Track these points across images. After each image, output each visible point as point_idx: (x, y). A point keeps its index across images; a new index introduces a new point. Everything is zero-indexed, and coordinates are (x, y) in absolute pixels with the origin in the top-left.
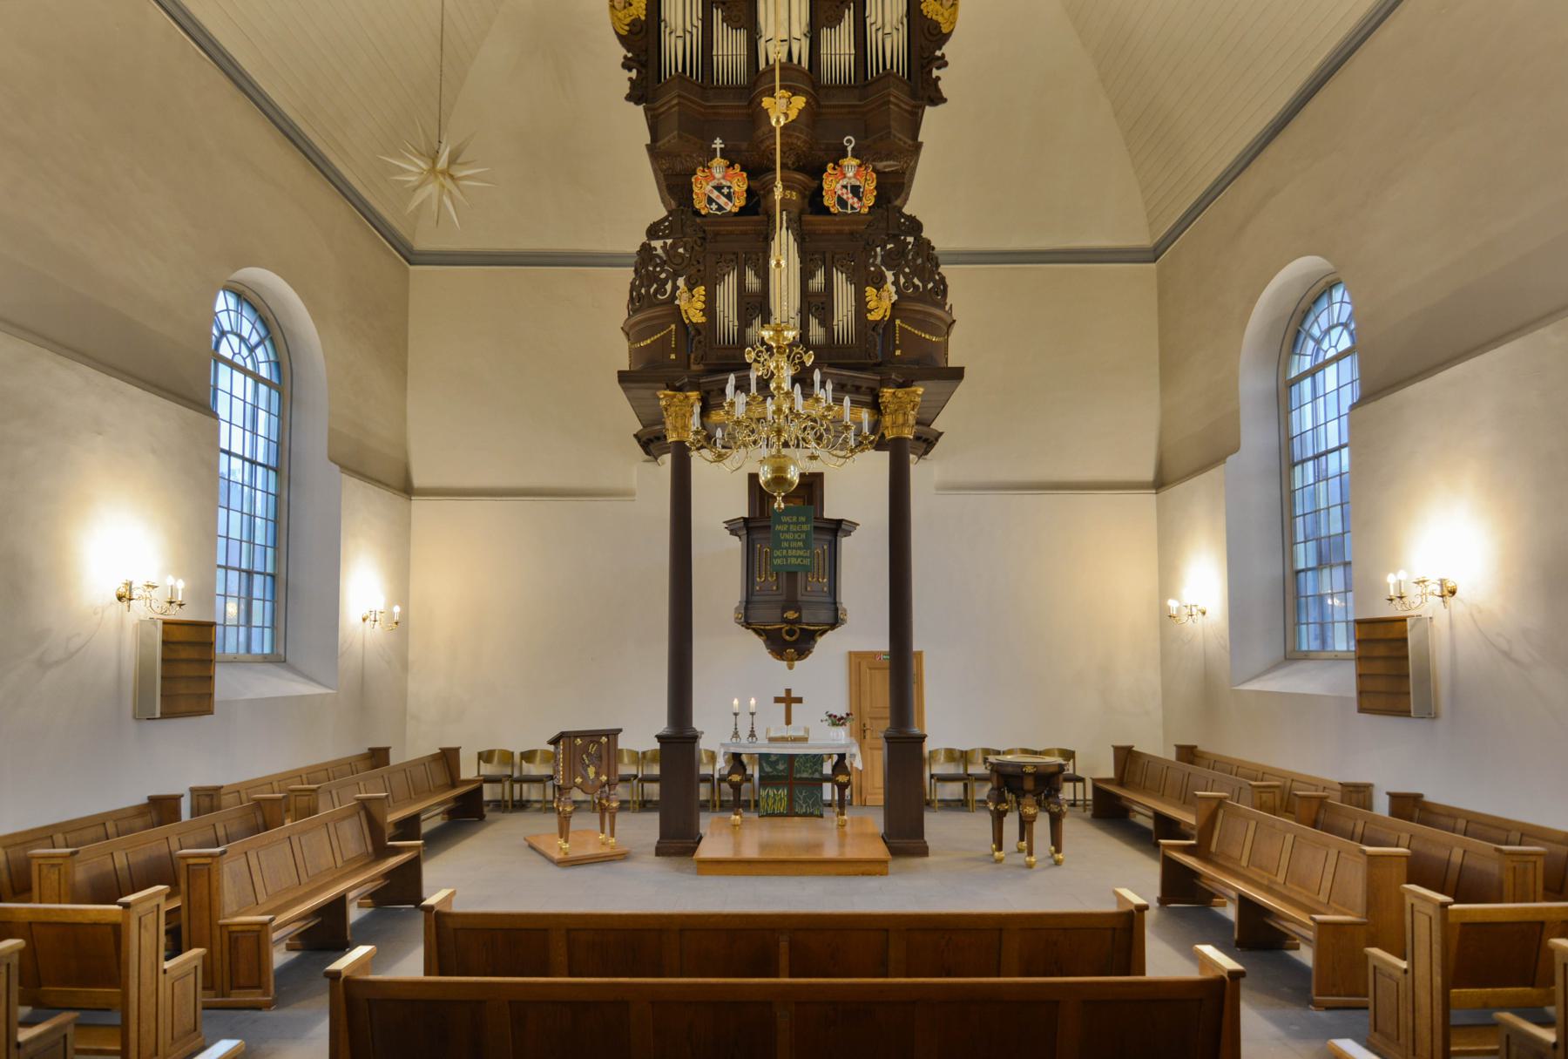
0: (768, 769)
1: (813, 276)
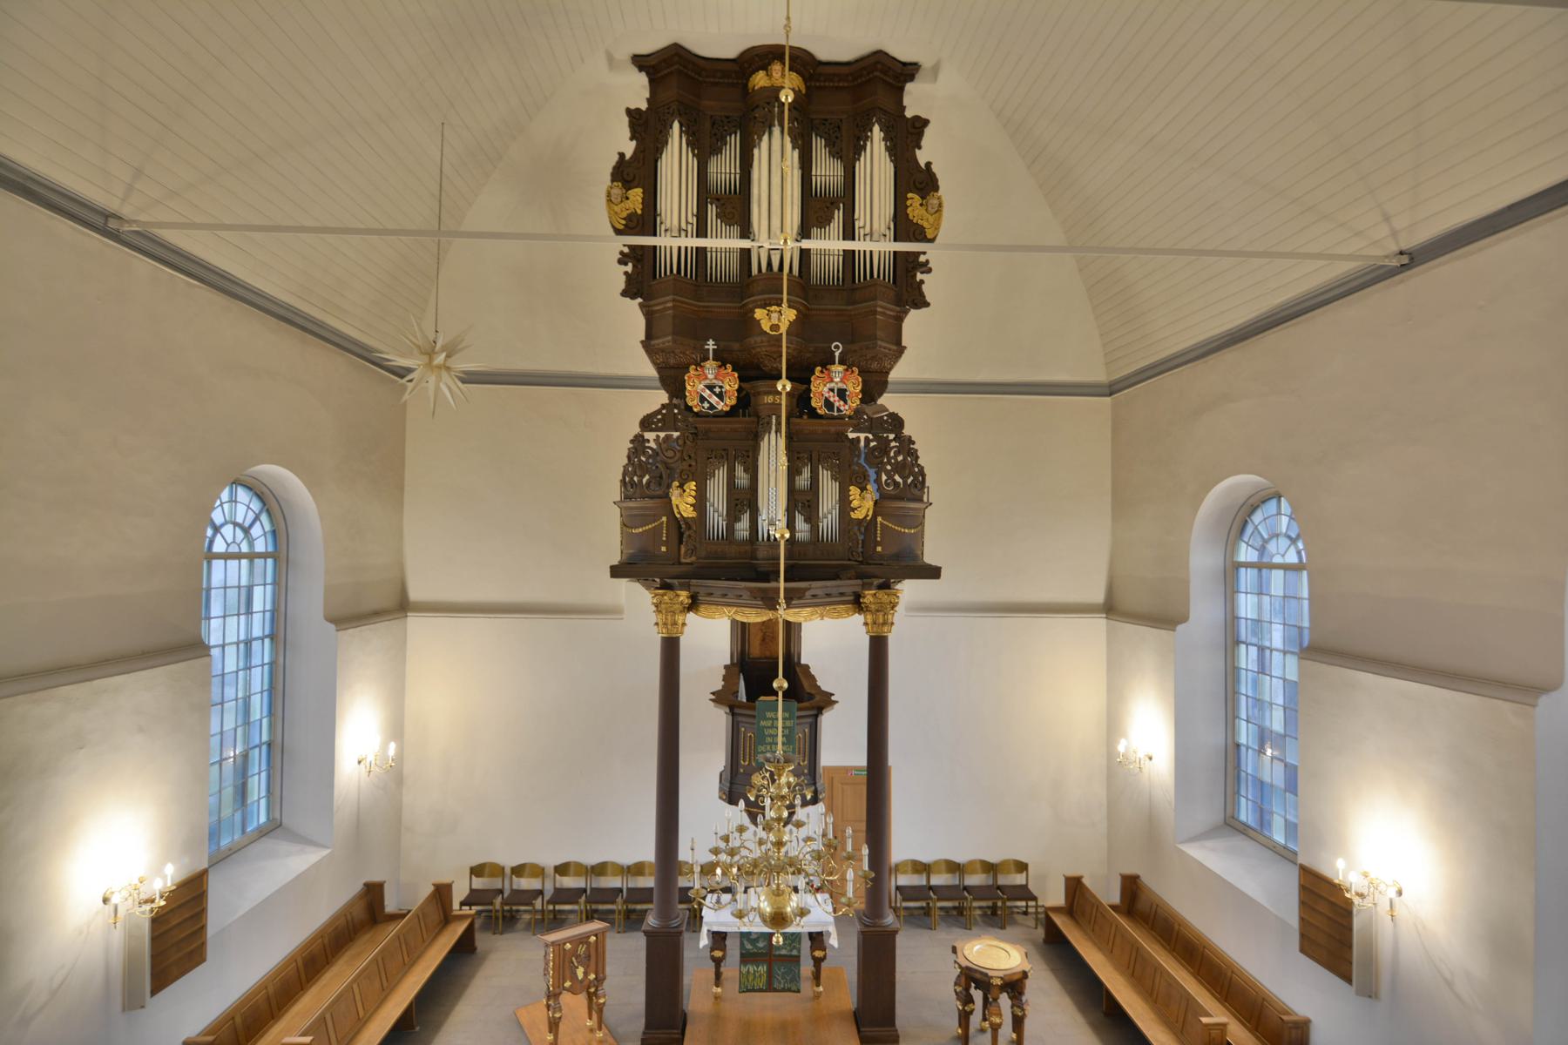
0: (749, 946)
1: (800, 473)
